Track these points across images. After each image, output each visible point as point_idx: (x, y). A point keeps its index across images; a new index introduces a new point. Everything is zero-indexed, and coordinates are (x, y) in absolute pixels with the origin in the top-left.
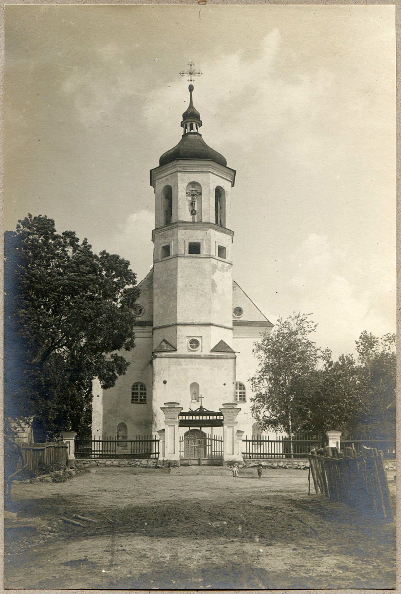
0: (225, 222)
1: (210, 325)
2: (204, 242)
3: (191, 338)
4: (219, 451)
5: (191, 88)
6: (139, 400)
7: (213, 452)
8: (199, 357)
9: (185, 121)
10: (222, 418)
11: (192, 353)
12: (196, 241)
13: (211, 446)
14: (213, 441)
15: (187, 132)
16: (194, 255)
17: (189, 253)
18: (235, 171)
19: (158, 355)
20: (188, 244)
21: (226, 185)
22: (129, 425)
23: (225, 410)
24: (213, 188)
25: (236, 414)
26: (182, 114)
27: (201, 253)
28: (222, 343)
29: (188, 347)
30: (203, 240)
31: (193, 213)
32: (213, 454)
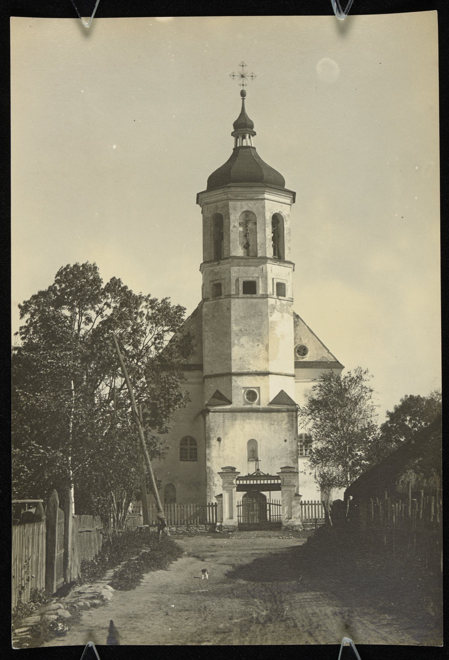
0: (284, 253)
1: (266, 374)
2: (260, 280)
3: (248, 389)
4: (275, 516)
5: (243, 94)
6: (189, 457)
7: (272, 517)
8: (257, 411)
9: (237, 132)
10: (280, 481)
11: (248, 406)
12: (251, 279)
13: (270, 510)
14: (271, 505)
15: (238, 146)
16: (249, 295)
17: (244, 293)
18: (294, 194)
19: (212, 409)
20: (242, 283)
21: (285, 211)
22: (178, 486)
23: (283, 474)
24: (269, 216)
25: (293, 477)
26: (233, 123)
27: (257, 292)
28: (282, 394)
29: (244, 399)
30: (259, 278)
31: (246, 246)
32: (272, 519)
